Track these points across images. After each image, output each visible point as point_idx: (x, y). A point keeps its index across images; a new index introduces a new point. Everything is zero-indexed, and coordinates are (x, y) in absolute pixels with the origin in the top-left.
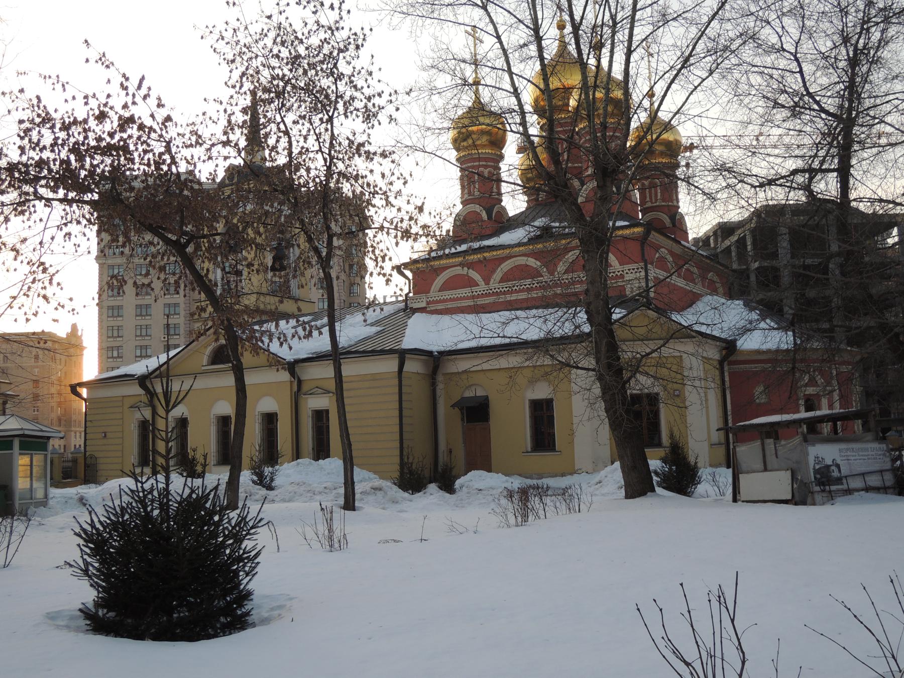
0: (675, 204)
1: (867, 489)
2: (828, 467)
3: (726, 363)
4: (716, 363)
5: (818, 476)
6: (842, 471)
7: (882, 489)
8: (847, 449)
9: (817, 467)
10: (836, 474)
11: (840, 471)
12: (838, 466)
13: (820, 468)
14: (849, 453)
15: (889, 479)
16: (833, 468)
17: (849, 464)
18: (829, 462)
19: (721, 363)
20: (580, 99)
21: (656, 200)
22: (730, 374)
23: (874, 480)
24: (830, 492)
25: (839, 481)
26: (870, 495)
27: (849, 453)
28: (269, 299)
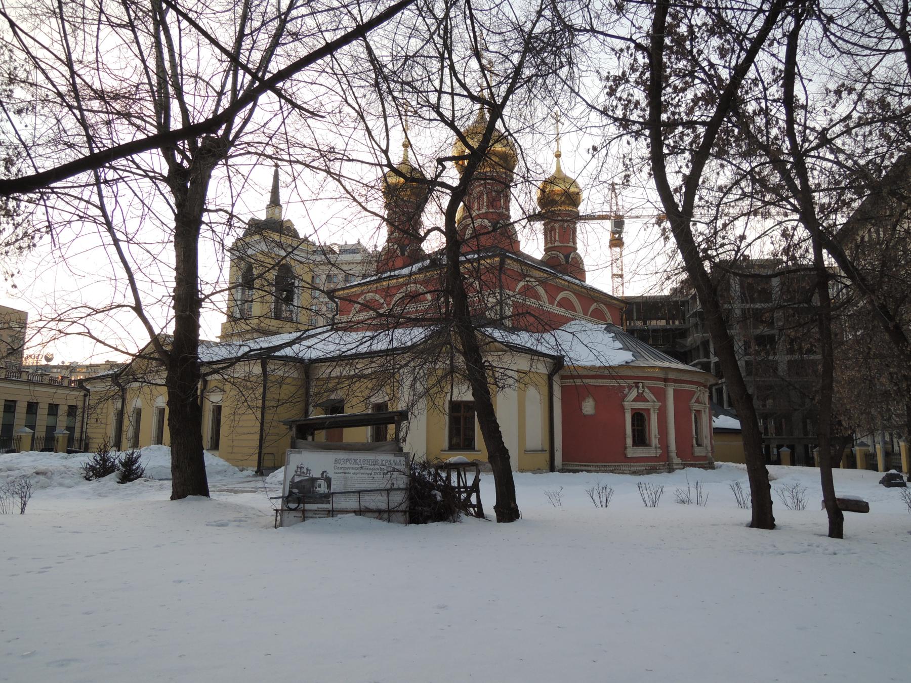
0: (571, 244)
1: (360, 512)
2: (313, 480)
3: (556, 378)
4: (546, 377)
5: (295, 491)
6: (332, 487)
7: (385, 514)
8: (347, 460)
9: (297, 479)
10: (322, 489)
11: (329, 486)
12: (328, 481)
13: (301, 482)
14: (348, 465)
15: (398, 498)
16: (322, 482)
17: (345, 479)
18: (316, 474)
19: (550, 377)
20: (155, 99)
21: (555, 241)
22: (564, 389)
23: (379, 501)
24: (304, 511)
25: (326, 497)
26: (360, 519)
27: (348, 465)
28: (267, 321)
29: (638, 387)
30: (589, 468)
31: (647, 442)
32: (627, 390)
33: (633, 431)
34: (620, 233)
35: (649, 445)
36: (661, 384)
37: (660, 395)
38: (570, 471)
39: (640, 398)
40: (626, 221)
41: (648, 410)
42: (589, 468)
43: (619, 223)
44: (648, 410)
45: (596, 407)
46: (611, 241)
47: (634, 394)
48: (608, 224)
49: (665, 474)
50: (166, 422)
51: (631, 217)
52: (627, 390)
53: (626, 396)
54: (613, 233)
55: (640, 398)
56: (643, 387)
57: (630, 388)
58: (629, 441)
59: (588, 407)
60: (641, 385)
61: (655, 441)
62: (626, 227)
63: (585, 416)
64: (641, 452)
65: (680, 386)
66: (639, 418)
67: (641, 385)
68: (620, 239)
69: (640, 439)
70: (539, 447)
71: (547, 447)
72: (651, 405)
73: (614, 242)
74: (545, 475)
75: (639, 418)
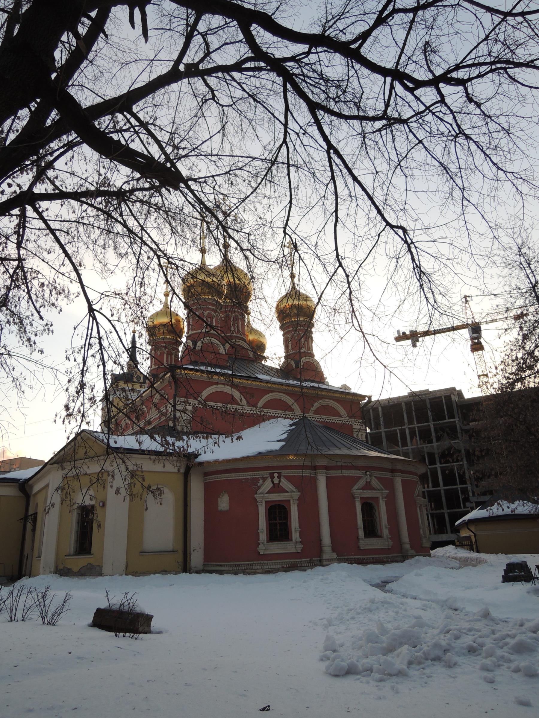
29: (272, 478)
30: (223, 568)
31: (379, 533)
32: (261, 482)
33: (364, 521)
34: (479, 337)
35: (380, 537)
36: (388, 475)
37: (389, 484)
38: (211, 572)
39: (277, 488)
40: (483, 327)
41: (377, 499)
42: (223, 568)
43: (476, 329)
44: (377, 499)
45: (230, 503)
46: (471, 346)
47: (268, 485)
48: (466, 333)
49: (242, 575)
50: (420, 518)
51: (487, 322)
52: (261, 482)
53: (259, 487)
54: (472, 339)
55: (368, 486)
56: (279, 477)
57: (264, 479)
58: (361, 533)
59: (224, 503)
60: (276, 475)
61: (386, 532)
62: (483, 333)
63: (222, 512)
64: (276, 548)
65: (333, 473)
66: (369, 508)
67: (276, 475)
68: (480, 343)
69: (371, 531)
70: (170, 547)
71: (180, 547)
72: (380, 494)
73: (476, 346)
74: (171, 577)
75: (369, 508)
